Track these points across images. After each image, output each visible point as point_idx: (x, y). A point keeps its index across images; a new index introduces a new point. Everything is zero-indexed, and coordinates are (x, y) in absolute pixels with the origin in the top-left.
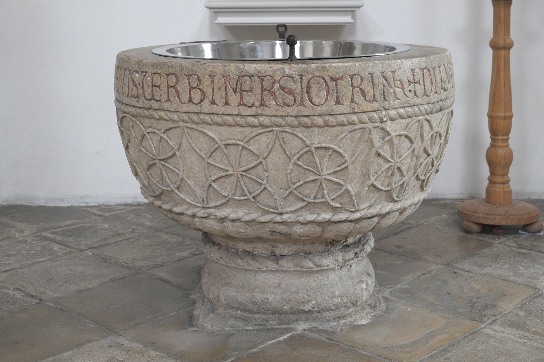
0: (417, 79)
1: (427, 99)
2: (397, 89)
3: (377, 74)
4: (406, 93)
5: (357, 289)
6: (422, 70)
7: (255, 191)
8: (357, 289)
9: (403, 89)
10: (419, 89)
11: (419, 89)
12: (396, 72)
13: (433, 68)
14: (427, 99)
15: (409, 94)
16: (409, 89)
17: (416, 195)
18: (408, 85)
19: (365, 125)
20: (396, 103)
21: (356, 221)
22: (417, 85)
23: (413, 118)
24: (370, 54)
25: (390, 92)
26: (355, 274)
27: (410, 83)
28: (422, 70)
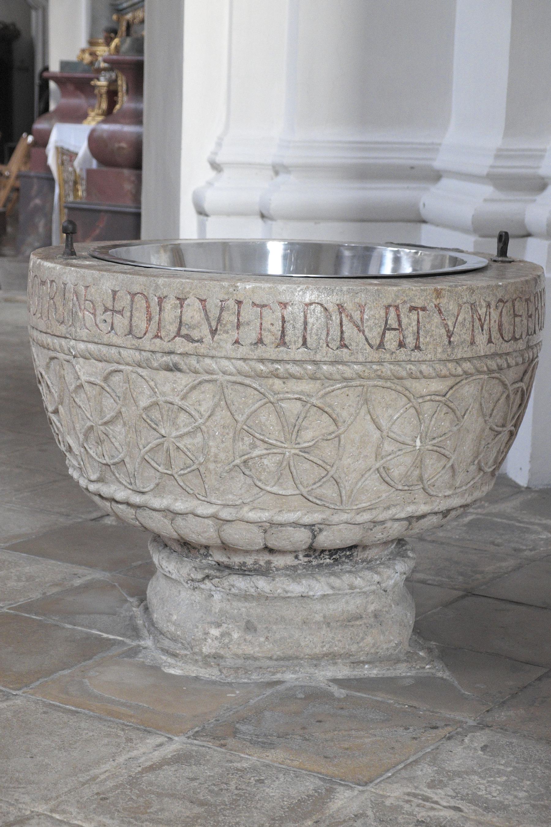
0: (118, 307)
1: (134, 342)
2: (87, 313)
3: (70, 286)
4: (98, 322)
5: (197, 628)
6: (133, 295)
7: (370, 475)
8: (197, 628)
9: (94, 314)
10: (121, 322)
11: (121, 322)
12: (89, 288)
13: (159, 298)
14: (134, 342)
15: (102, 326)
16: (103, 317)
17: (181, 499)
18: (102, 313)
19: (214, 377)
20: (83, 333)
21: (137, 507)
22: (118, 317)
23: (112, 364)
24: (307, 274)
25: (78, 316)
26: (217, 611)
27: (106, 310)
28: (133, 295)
